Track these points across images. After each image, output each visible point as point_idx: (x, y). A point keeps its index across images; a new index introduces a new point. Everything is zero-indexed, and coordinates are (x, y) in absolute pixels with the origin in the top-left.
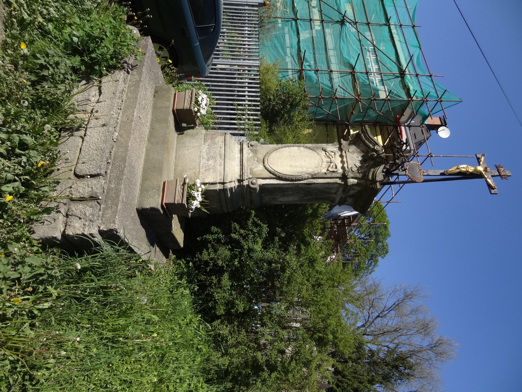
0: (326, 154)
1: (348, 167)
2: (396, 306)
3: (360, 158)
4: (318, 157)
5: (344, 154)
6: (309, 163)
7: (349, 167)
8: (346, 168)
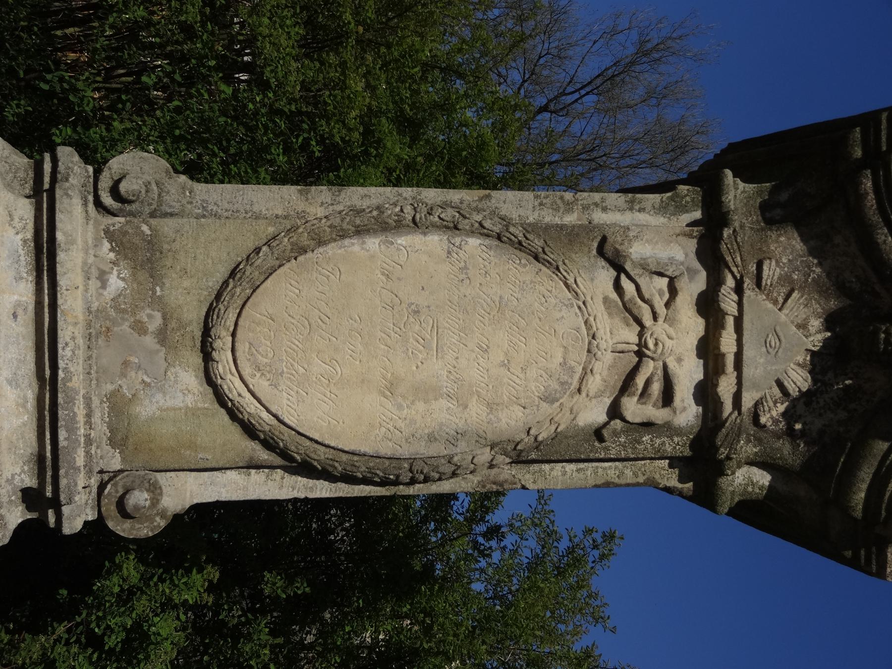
2: (608, 81)
3: (816, 338)
4: (572, 319)
5: (728, 303)
6: (505, 365)
7: (748, 401)
8: (728, 407)
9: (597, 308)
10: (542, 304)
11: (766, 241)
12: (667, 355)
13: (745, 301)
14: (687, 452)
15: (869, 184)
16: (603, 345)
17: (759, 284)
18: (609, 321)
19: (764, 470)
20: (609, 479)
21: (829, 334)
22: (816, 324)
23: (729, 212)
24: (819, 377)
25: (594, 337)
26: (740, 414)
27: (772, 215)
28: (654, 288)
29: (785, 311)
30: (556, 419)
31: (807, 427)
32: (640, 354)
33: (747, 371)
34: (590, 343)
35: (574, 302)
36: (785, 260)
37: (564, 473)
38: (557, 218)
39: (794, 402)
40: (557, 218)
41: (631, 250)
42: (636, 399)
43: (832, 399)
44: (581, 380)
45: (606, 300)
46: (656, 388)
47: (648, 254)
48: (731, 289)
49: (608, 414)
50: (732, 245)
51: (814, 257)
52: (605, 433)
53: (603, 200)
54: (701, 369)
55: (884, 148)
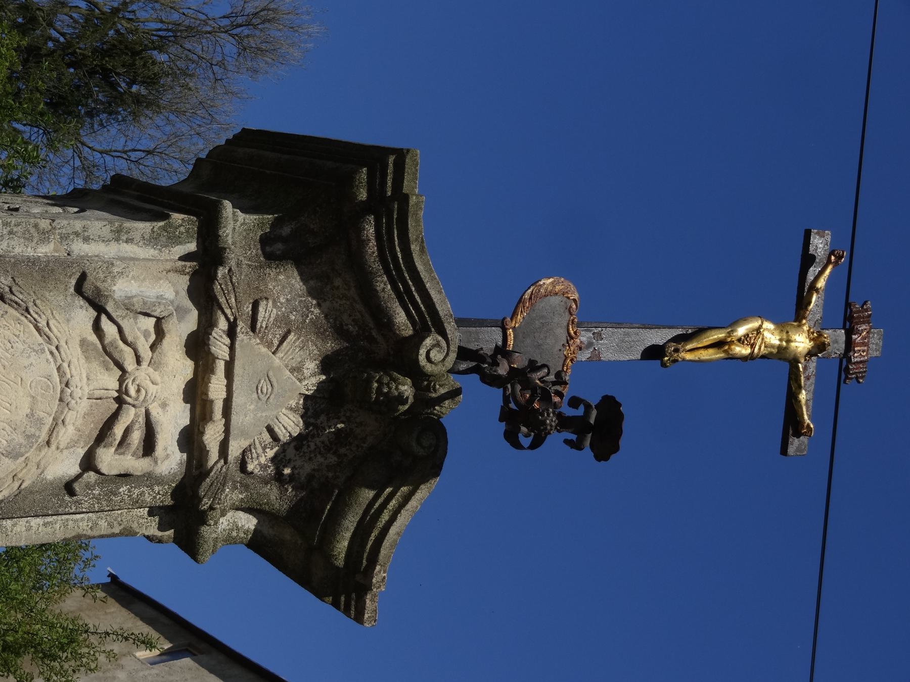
0: (97, 328)
1: (224, 446)
3: (311, 382)
4: (44, 366)
5: (219, 346)
7: (235, 450)
9: (73, 353)
10: (7, 351)
11: (263, 279)
12: (150, 402)
13: (237, 346)
14: (169, 501)
15: (372, 230)
16: (78, 393)
17: (253, 328)
18: (86, 365)
19: (250, 514)
20: (80, 531)
21: (324, 377)
22: (311, 366)
23: (225, 249)
24: (312, 420)
25: (67, 385)
26: (226, 463)
27: (273, 250)
28: (139, 329)
29: (280, 354)
30: (20, 476)
31: (296, 472)
32: (120, 401)
33: (235, 419)
34: (62, 391)
35: (46, 347)
36: (282, 300)
37: (29, 528)
38: (29, 249)
39: (284, 447)
40: (29, 249)
41: (114, 288)
42: (113, 449)
43: (323, 442)
44: (52, 431)
45: (83, 343)
46: (137, 437)
47: (134, 293)
48: (224, 331)
49: (81, 465)
50: (226, 285)
51: (313, 298)
52: (77, 487)
53: (85, 229)
54: (187, 414)
55: (389, 194)
